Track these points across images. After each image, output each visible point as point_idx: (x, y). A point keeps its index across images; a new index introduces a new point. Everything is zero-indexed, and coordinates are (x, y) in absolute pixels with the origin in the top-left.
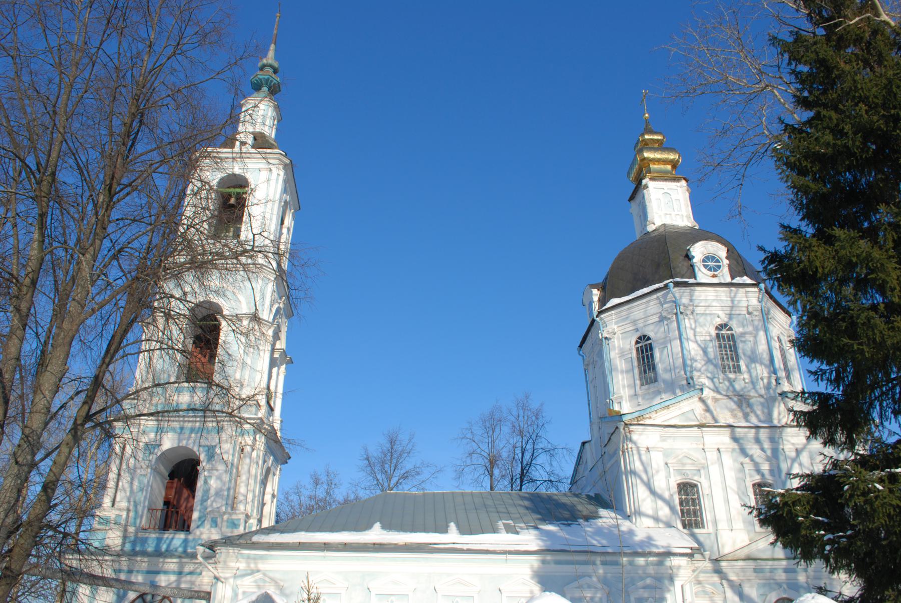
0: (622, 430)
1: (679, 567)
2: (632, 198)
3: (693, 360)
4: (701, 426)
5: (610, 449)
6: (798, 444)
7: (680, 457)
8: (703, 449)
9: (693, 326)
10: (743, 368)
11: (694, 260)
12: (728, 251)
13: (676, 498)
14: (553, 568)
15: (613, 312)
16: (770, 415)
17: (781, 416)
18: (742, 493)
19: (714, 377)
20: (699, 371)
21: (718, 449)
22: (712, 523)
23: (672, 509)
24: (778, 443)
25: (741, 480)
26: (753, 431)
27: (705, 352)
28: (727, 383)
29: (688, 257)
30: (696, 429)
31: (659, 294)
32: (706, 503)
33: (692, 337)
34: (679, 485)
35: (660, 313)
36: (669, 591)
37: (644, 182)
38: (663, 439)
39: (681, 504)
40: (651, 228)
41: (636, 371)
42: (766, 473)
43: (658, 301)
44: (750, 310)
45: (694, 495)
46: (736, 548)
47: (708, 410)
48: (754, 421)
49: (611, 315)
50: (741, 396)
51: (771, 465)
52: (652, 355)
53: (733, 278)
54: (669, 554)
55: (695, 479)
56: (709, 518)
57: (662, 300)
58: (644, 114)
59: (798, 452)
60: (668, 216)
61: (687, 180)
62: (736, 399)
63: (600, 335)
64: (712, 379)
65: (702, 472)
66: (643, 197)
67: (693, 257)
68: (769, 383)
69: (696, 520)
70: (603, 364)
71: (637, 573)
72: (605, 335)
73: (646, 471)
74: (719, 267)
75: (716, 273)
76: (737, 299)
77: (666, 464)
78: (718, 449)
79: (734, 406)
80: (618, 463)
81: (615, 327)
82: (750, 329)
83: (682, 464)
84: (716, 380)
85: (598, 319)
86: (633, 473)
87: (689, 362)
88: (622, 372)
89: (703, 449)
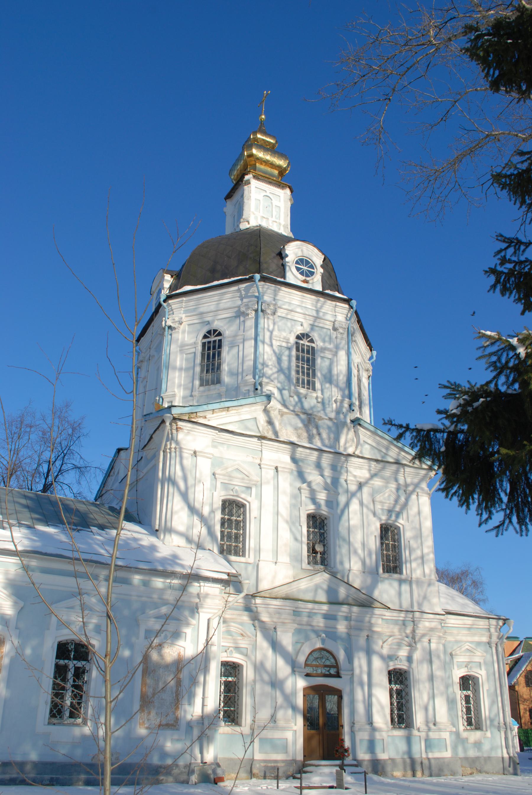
0: (168, 424)
1: (207, 595)
2: (229, 196)
3: (264, 364)
4: (262, 438)
5: (148, 453)
6: (360, 477)
7: (229, 470)
8: (259, 465)
9: (271, 328)
10: (318, 385)
11: (287, 259)
12: (324, 259)
13: (218, 516)
14: (38, 577)
15: (184, 299)
16: (337, 439)
17: (348, 445)
18: (292, 522)
19: (284, 389)
20: (269, 378)
21: (276, 468)
22: (255, 551)
23: (211, 532)
24: (340, 473)
25: (295, 506)
26: (316, 453)
27: (279, 360)
28: (296, 398)
29: (281, 255)
30: (255, 440)
31: (243, 286)
32: (251, 528)
33: (267, 340)
34: (224, 502)
35: (239, 307)
36: (188, 624)
37: (247, 177)
38: (215, 444)
39: (222, 524)
40: (244, 226)
41: (198, 369)
42: (323, 503)
43: (238, 294)
44: (337, 325)
45: (239, 516)
46: (277, 584)
47: (270, 422)
48: (318, 443)
49: (181, 302)
50: (310, 415)
51: (328, 496)
52: (219, 354)
53: (324, 288)
54: (197, 577)
55: (243, 497)
56: (252, 545)
57: (243, 293)
58: (261, 115)
59: (361, 486)
60: (264, 220)
61: (292, 191)
62: (303, 416)
63: (164, 323)
64: (280, 390)
65: (254, 490)
66: (242, 196)
67: (287, 256)
68: (341, 406)
69: (237, 546)
70: (160, 357)
71: (151, 598)
72: (169, 323)
73: (185, 479)
74: (312, 274)
75: (308, 279)
76: (323, 311)
77: (214, 474)
78: (276, 468)
79: (300, 425)
80: (155, 468)
81: (183, 316)
82: (331, 346)
83: (230, 476)
84: (286, 393)
85: (165, 305)
86: (172, 481)
87: (260, 366)
88: (181, 369)
89: (259, 465)
